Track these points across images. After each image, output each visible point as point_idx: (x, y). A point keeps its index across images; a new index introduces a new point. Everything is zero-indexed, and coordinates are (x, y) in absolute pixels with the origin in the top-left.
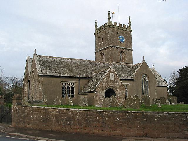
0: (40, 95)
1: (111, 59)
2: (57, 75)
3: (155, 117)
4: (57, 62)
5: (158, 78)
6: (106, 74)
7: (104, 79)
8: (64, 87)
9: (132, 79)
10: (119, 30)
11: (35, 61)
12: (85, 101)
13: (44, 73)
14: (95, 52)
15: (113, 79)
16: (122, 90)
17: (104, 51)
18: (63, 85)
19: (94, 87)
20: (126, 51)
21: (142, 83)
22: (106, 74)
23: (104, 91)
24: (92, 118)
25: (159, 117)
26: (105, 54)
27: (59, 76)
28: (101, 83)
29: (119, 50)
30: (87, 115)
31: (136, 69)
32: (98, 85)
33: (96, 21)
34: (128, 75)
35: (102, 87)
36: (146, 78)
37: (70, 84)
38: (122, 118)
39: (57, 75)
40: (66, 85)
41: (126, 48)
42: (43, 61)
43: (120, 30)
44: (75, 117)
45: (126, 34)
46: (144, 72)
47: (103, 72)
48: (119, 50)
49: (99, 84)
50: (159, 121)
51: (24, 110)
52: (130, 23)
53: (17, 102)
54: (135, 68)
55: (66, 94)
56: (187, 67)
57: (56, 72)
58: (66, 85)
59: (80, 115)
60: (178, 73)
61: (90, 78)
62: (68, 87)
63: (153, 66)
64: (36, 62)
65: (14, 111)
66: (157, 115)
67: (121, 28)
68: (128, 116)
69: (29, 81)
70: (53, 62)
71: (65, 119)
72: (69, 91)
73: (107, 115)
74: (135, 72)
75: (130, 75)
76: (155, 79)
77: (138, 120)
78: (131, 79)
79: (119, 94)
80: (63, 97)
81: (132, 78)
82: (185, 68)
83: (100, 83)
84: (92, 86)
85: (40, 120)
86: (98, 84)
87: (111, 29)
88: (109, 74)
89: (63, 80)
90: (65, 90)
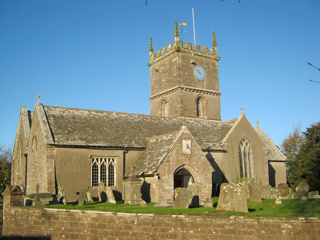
0: (50, 183)
1: (181, 111)
2: (83, 143)
3: (283, 227)
4: (80, 119)
5: (269, 147)
6: (175, 141)
7: (172, 150)
8: (95, 167)
10: (195, 56)
11: (39, 116)
12: (137, 194)
15: (188, 152)
16: (205, 171)
17: (168, 96)
18: (94, 162)
19: (152, 166)
21: (240, 156)
22: (175, 141)
23: (171, 173)
24: (163, 230)
25: (290, 226)
26: (170, 101)
27: (86, 146)
28: (166, 158)
29: (196, 94)
30: (153, 226)
31: (229, 129)
32: (161, 163)
34: (214, 142)
37: (107, 160)
38: (219, 229)
39: (82, 145)
40: (99, 162)
42: (54, 116)
43: (197, 57)
44: (130, 228)
45: (208, 64)
47: (168, 138)
48: (196, 94)
49: (163, 160)
50: (289, 234)
51: (28, 217)
52: (311, 126)
53: (12, 201)
54: (225, 129)
55: (99, 179)
56: (319, 124)
57: (81, 139)
58: (99, 162)
59: (139, 224)
60: (304, 136)
61: (143, 149)
62: (103, 166)
63: (258, 122)
64: (40, 119)
65: (6, 218)
66: (286, 223)
67: (198, 52)
68: (231, 225)
69: (26, 155)
70: (74, 118)
71: (111, 232)
72: (112, 177)
73: (192, 223)
74: (227, 136)
75: (217, 142)
77: (251, 233)
78: (220, 148)
80: (93, 185)
81: (222, 147)
82: (317, 125)
84: (149, 165)
85: (61, 234)
86: (161, 160)
87: (180, 54)
89: (93, 152)
90: (98, 173)
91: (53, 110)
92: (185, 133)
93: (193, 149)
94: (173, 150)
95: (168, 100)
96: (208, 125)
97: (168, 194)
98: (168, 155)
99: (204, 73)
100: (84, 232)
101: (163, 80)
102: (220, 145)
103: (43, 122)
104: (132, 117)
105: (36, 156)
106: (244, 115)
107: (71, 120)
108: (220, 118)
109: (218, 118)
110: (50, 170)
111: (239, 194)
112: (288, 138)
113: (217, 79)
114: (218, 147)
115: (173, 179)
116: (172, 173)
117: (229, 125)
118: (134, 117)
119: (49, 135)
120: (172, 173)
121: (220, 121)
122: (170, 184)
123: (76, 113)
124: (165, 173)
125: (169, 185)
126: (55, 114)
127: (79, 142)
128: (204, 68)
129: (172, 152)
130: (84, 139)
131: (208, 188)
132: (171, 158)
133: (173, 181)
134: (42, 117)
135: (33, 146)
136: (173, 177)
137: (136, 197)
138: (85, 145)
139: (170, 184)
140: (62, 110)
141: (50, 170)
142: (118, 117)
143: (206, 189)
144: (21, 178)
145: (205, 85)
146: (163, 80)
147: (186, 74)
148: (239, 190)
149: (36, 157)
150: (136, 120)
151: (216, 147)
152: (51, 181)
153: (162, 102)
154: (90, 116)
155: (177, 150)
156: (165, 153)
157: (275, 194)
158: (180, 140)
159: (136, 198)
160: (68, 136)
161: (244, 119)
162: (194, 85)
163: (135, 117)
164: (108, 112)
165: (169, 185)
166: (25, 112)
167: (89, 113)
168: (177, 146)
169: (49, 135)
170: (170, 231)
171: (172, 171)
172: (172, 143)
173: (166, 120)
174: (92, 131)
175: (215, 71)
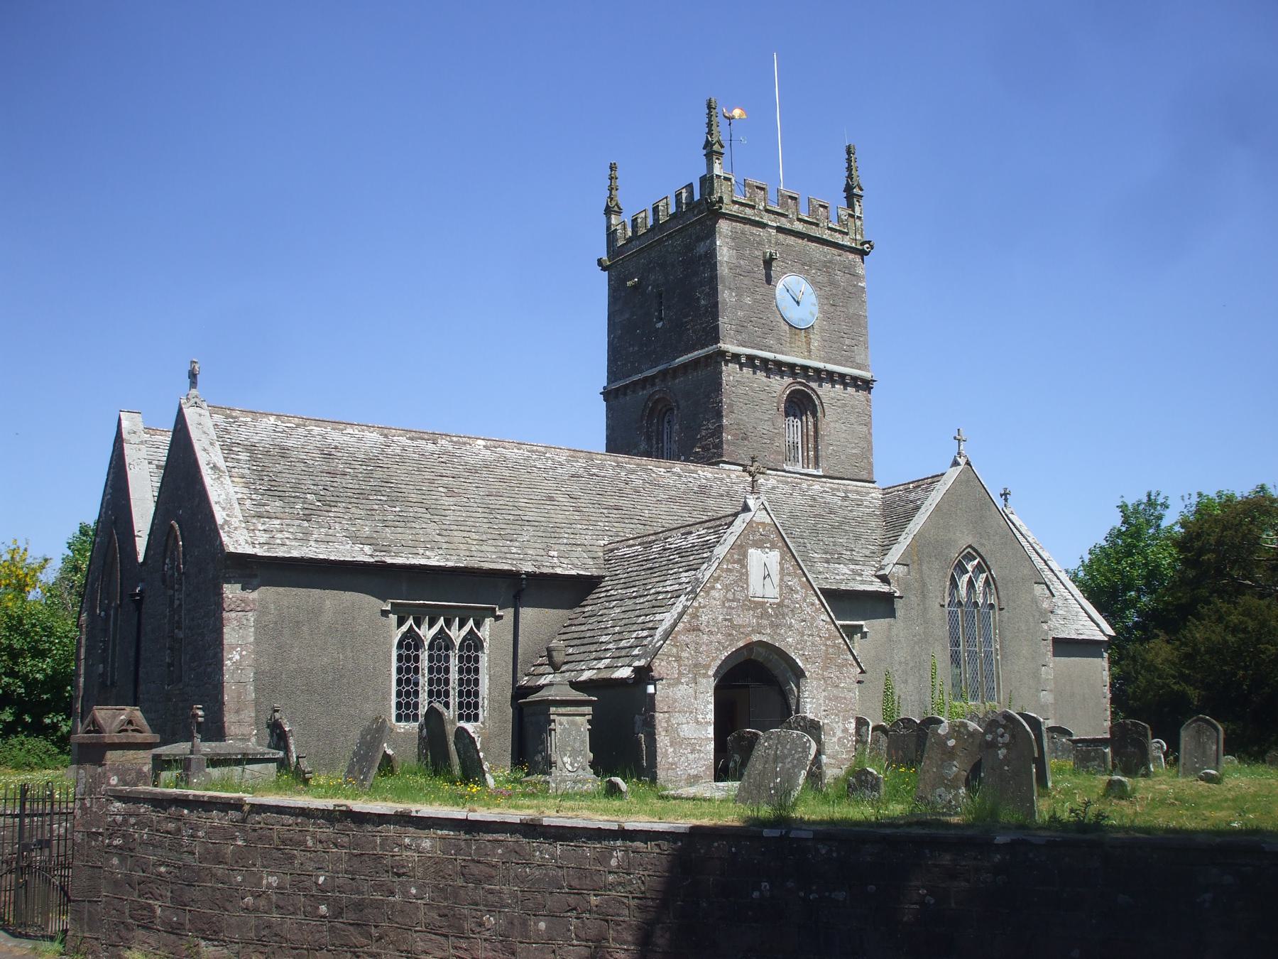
6: (721, 551)
9: (885, 588)
12: (574, 754)
13: (263, 538)
14: (607, 394)
20: (826, 392)
23: (705, 676)
28: (686, 618)
29: (781, 386)
31: (909, 516)
33: (613, 167)
34: (856, 563)
35: (692, 646)
36: (980, 584)
41: (830, 367)
45: (827, 266)
46: (964, 540)
49: (675, 625)
57: (355, 539)
62: (442, 641)
76: (1039, 590)
79: (812, 703)
80: (399, 718)
83: (681, 615)
86: (666, 625)
88: (745, 555)
91: (245, 424)
92: (758, 524)
93: (787, 586)
94: (713, 588)
95: (676, 401)
96: (828, 498)
97: (691, 757)
98: (696, 604)
99: (813, 299)
100: (405, 893)
101: (659, 325)
102: (879, 573)
103: (211, 468)
104: (547, 459)
105: (177, 602)
106: (968, 463)
107: (319, 464)
108: (870, 472)
109: (864, 475)
110: (238, 657)
111: (1002, 753)
112: (1087, 558)
113: (857, 322)
114: (871, 583)
115: (712, 700)
116: (710, 677)
117: (911, 499)
118: (553, 460)
119: (233, 520)
120: (710, 677)
121: (871, 485)
122: (700, 717)
123: (335, 437)
124: (680, 673)
125: (697, 722)
126: (256, 439)
127: (348, 547)
128: (813, 283)
129: (708, 593)
130: (368, 541)
131: (839, 734)
132: (704, 618)
133: (712, 707)
134: (205, 450)
135: (167, 561)
136: (711, 692)
137: (572, 765)
138: (372, 560)
139: (701, 716)
140: (281, 426)
141: (238, 657)
142: (494, 456)
143: (835, 739)
144: (113, 684)
145: (815, 344)
146: (659, 325)
147: (748, 300)
148: (1002, 736)
149: (180, 605)
150: (560, 471)
151: (863, 582)
152: (239, 697)
153: (652, 410)
154: (389, 451)
155: (727, 588)
156: (683, 598)
157: (1096, 763)
158: (740, 550)
159: (570, 768)
160: (306, 524)
161: (969, 479)
162: (776, 347)
163: (556, 458)
164: (455, 439)
165: (697, 722)
166: (135, 433)
167: (382, 439)
168: (728, 570)
169: (233, 520)
170: (756, 894)
171: (707, 667)
172: (709, 559)
173: (674, 473)
174: (398, 509)
175: (854, 294)
